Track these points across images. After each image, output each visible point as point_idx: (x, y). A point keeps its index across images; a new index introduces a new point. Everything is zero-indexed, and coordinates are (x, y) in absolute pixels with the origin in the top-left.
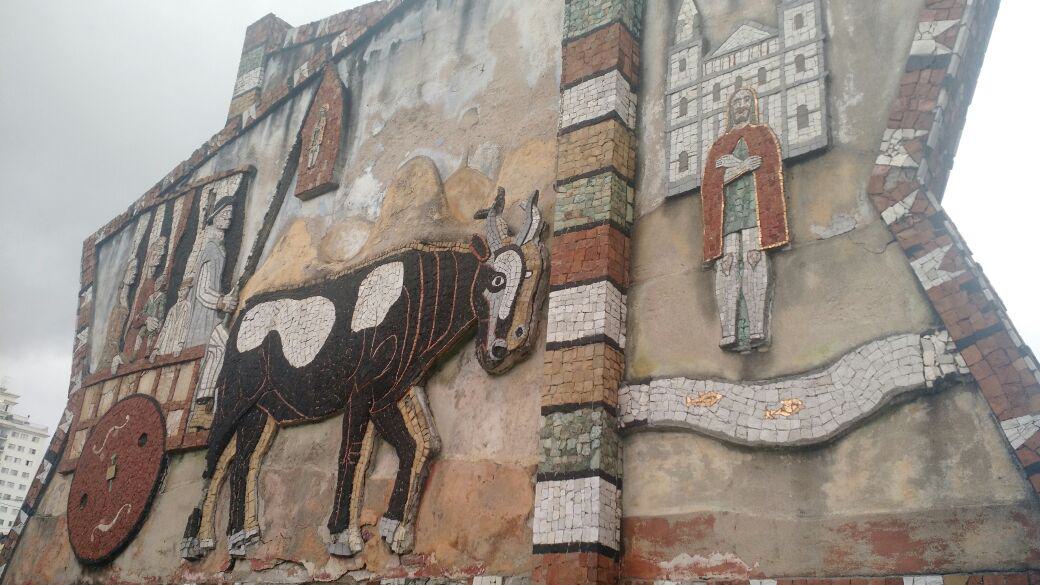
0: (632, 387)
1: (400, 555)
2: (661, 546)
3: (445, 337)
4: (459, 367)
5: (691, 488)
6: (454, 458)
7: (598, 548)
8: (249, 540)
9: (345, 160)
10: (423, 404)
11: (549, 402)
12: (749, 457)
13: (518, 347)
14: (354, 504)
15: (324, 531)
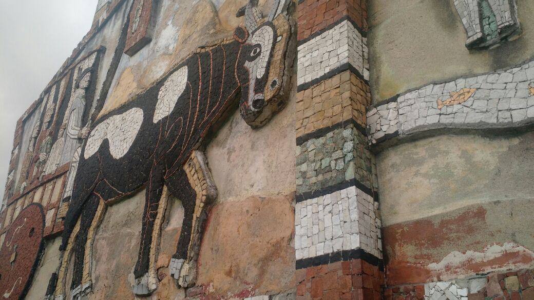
0: (379, 108)
1: (186, 289)
2: (427, 248)
3: (217, 108)
4: (230, 130)
5: (452, 186)
6: (229, 201)
7: (359, 253)
8: (84, 292)
9: (155, 22)
10: (202, 163)
11: (302, 132)
12: (516, 141)
13: (274, 96)
14: (152, 252)
15: (132, 276)
